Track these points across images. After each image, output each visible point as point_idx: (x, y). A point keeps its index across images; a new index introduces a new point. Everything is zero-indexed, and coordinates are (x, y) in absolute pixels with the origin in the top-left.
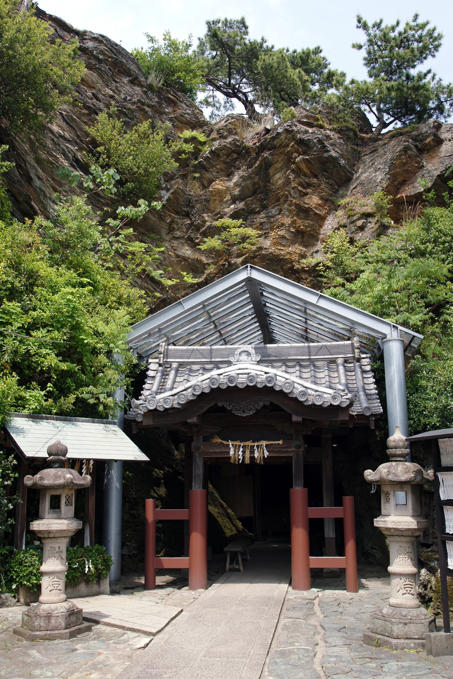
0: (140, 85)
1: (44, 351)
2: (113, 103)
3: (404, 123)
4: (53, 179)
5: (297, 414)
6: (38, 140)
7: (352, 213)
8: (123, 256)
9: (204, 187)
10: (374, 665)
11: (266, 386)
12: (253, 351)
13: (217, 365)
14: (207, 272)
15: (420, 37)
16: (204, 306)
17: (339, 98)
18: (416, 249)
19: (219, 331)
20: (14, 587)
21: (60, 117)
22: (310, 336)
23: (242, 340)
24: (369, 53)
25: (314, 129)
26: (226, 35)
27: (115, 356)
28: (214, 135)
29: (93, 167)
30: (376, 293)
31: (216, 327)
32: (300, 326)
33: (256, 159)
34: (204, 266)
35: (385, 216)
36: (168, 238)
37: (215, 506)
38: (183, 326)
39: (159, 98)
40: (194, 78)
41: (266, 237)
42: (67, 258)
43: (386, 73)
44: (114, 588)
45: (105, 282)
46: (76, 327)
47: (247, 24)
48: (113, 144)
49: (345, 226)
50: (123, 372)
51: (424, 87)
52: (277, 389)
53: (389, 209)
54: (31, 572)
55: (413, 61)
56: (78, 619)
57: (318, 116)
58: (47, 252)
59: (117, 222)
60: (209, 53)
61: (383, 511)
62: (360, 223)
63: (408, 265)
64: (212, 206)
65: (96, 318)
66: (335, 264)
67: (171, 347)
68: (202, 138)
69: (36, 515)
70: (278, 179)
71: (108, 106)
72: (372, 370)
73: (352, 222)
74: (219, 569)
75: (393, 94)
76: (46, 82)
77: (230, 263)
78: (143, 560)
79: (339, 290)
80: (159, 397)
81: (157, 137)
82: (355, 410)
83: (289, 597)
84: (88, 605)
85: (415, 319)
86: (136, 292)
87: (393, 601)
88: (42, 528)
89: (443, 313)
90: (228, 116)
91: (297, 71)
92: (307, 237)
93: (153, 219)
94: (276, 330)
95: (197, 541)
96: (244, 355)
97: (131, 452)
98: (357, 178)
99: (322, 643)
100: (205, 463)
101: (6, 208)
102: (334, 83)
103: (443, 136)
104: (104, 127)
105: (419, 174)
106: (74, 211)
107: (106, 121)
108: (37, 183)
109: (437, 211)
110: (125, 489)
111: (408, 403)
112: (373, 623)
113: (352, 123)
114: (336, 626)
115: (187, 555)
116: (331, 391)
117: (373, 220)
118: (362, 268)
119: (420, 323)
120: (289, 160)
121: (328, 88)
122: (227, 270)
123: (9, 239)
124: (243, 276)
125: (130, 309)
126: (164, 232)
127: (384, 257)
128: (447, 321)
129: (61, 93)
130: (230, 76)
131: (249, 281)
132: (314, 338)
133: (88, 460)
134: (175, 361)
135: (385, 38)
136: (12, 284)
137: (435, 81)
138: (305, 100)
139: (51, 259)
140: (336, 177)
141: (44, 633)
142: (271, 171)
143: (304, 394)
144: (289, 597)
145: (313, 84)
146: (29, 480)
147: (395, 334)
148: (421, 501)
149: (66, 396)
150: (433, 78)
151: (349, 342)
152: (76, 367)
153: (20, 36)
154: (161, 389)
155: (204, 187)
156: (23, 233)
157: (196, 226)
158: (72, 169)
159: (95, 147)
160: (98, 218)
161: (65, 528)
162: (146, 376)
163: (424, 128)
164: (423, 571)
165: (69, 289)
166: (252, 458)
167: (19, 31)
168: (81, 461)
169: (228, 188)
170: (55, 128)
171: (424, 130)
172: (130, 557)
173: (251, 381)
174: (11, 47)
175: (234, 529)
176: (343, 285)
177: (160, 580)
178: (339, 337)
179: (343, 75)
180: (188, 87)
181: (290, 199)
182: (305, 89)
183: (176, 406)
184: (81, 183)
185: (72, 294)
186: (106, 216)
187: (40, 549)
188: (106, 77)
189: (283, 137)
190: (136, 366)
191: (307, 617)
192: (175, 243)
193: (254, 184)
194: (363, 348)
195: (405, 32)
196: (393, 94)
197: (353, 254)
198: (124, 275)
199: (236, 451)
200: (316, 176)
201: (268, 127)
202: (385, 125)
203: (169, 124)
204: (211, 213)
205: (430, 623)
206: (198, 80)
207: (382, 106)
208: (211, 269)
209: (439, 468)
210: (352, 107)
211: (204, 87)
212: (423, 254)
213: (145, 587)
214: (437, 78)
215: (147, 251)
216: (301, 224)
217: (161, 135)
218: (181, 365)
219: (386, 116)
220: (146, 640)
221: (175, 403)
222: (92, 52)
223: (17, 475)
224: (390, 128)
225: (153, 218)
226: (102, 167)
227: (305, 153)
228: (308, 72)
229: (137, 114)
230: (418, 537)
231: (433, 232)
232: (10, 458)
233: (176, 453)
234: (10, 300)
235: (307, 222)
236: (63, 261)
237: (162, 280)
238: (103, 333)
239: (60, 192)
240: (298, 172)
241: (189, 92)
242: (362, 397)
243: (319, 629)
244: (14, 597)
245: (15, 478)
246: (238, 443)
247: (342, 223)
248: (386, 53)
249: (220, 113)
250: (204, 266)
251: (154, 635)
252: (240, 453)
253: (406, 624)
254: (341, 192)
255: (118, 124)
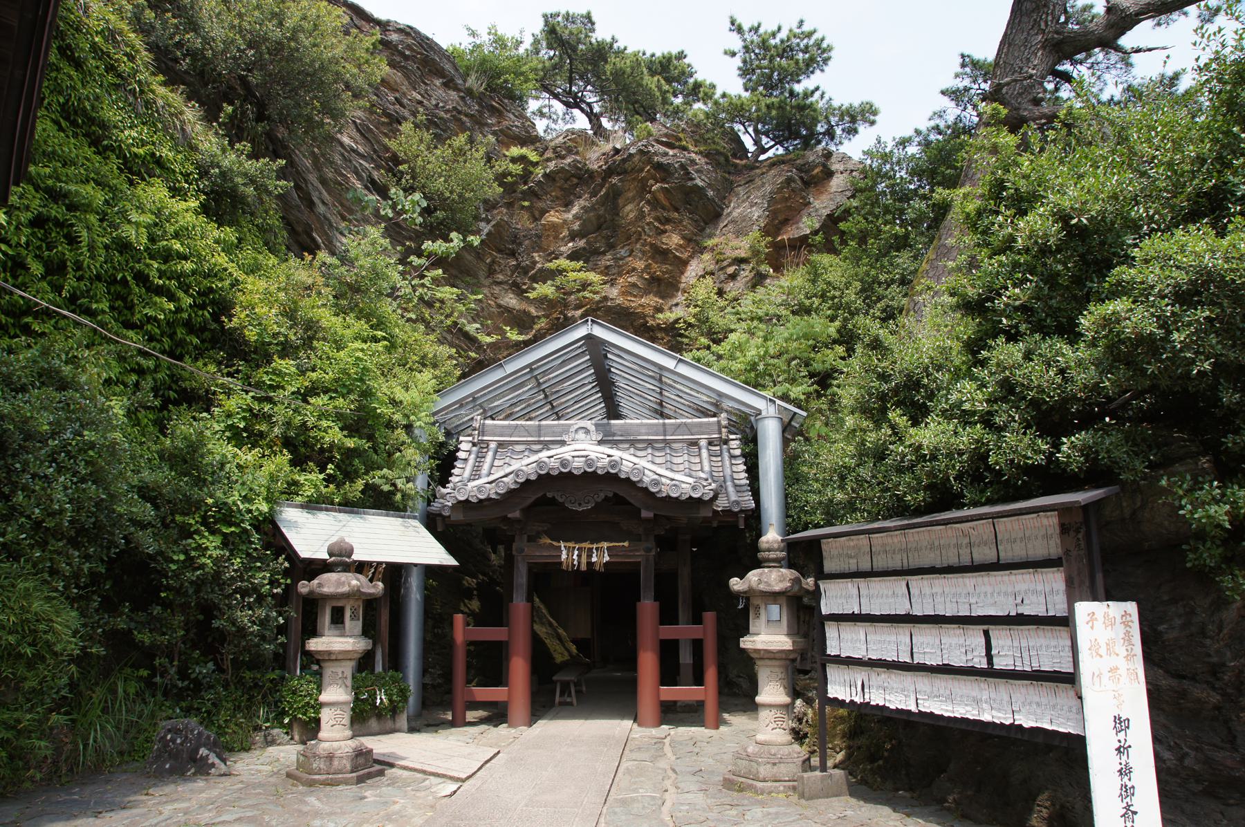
0: (457, 89)
1: (324, 423)
2: (421, 110)
3: (786, 149)
4: (342, 205)
5: (647, 508)
6: (323, 155)
7: (722, 257)
8: (430, 304)
9: (535, 219)
10: (734, 812)
11: (608, 472)
12: (593, 428)
13: (546, 445)
14: (537, 327)
15: (807, 47)
16: (532, 370)
17: (707, 114)
18: (799, 304)
19: (550, 403)
20: (286, 721)
21: (353, 126)
22: (666, 411)
23: (578, 414)
24: (745, 62)
25: (676, 151)
26: (567, 32)
27: (417, 432)
28: (549, 154)
29: (393, 190)
30: (749, 359)
31: (546, 397)
32: (653, 398)
33: (602, 186)
34: (533, 320)
35: (762, 262)
36: (487, 282)
37: (542, 624)
38: (502, 395)
39: (480, 105)
40: (526, 82)
41: (612, 285)
42: (357, 305)
43: (765, 88)
44: (413, 724)
45: (405, 338)
46: (367, 394)
47: (594, 19)
48: (419, 162)
49: (712, 274)
50: (426, 451)
51: (810, 106)
52: (623, 476)
53: (767, 254)
54: (308, 703)
55: (798, 75)
56: (367, 760)
57: (681, 135)
58: (331, 297)
59: (422, 261)
60: (546, 53)
61: (752, 629)
62: (731, 270)
63: (788, 325)
64: (544, 243)
65: (393, 383)
66: (699, 320)
67: (489, 422)
68: (534, 157)
69: (312, 631)
70: (629, 211)
71: (414, 114)
72: (743, 455)
73: (722, 269)
74: (544, 702)
75: (774, 113)
76: (335, 82)
77: (565, 316)
78: (450, 692)
79: (705, 353)
80: (471, 484)
81: (476, 155)
82: (721, 504)
83: (633, 735)
84: (380, 745)
85: (797, 391)
86: (445, 350)
87: (760, 737)
88: (320, 648)
89: (831, 385)
90: (568, 131)
91: (656, 79)
92: (665, 286)
93: (469, 258)
94: (623, 403)
95: (519, 668)
96: (581, 432)
97: (434, 553)
98: (729, 214)
99: (672, 790)
100: (530, 570)
101: (280, 240)
102: (701, 95)
103: (833, 168)
104: (409, 139)
105: (805, 212)
106: (366, 246)
107: (411, 133)
108: (321, 209)
109: (825, 259)
110: (427, 601)
111: (786, 496)
112: (735, 764)
113: (724, 145)
114: (690, 769)
115: (506, 685)
116: (691, 480)
117: (748, 267)
118: (733, 327)
119: (803, 397)
120: (644, 188)
121: (694, 101)
122: (561, 325)
123: (283, 278)
124: (581, 332)
125: (437, 372)
126: (482, 274)
127: (760, 313)
128: (834, 395)
129: (356, 96)
130: (571, 81)
131: (589, 338)
132: (671, 413)
133: (380, 563)
134: (493, 440)
135: (764, 45)
136: (286, 336)
137: (824, 100)
138: (665, 115)
139: (336, 305)
140: (704, 213)
141: (324, 777)
142: (621, 201)
143: (657, 483)
144: (633, 735)
145: (676, 96)
146: (304, 587)
147: (772, 410)
148: (798, 618)
149: (352, 481)
150: (822, 97)
151: (715, 419)
152: (365, 444)
153: (305, 25)
154: (475, 474)
155: (535, 219)
156: (300, 271)
157: (523, 268)
158: (366, 192)
159: (396, 166)
160: (398, 256)
161: (350, 648)
162: (456, 459)
163: (811, 157)
164: (799, 702)
165: (358, 345)
166: (590, 564)
167: (304, 18)
168: (370, 564)
169: (565, 221)
170: (346, 140)
171: (811, 159)
172: (433, 686)
173: (590, 466)
174: (294, 38)
175: (566, 653)
176: (708, 348)
177: (471, 715)
178: (705, 413)
179: (713, 86)
180: (518, 93)
181: (644, 237)
182: (665, 101)
183: (493, 496)
184: (377, 210)
185: (362, 350)
186: (408, 252)
187: (319, 674)
188: (413, 77)
189: (636, 159)
190: (442, 445)
191: (654, 759)
192: (497, 290)
193: (599, 217)
194: (733, 427)
195: (789, 39)
196: (774, 113)
197: (722, 309)
198: (430, 329)
199: (570, 555)
200: (677, 210)
201: (618, 146)
202: (764, 151)
203: (491, 138)
204: (544, 252)
205: (804, 762)
206: (530, 85)
207: (760, 126)
208: (542, 324)
209: (821, 575)
210: (723, 126)
211: (538, 94)
212: (808, 311)
213: (453, 724)
214: (827, 97)
215: (460, 299)
216: (658, 269)
217: (481, 153)
218: (501, 445)
219: (764, 140)
220: (454, 787)
221: (492, 492)
222: (396, 46)
223: (289, 581)
224: (770, 154)
225: (469, 257)
226: (405, 190)
227: (663, 180)
228: (669, 81)
229: (451, 125)
230: (794, 660)
231: (821, 286)
232: (281, 560)
233: (493, 556)
234: (282, 358)
235: (665, 267)
236: (352, 309)
237: (479, 337)
238: (401, 402)
239: (350, 221)
240: (655, 204)
241: (520, 100)
242: (731, 489)
243: (670, 773)
244: (287, 733)
245: (287, 585)
246: (571, 544)
247: (708, 269)
248: (765, 63)
249: (557, 127)
250: (533, 320)
251: (463, 781)
252: (575, 557)
253: (774, 764)
254: (708, 231)
255: (427, 136)
